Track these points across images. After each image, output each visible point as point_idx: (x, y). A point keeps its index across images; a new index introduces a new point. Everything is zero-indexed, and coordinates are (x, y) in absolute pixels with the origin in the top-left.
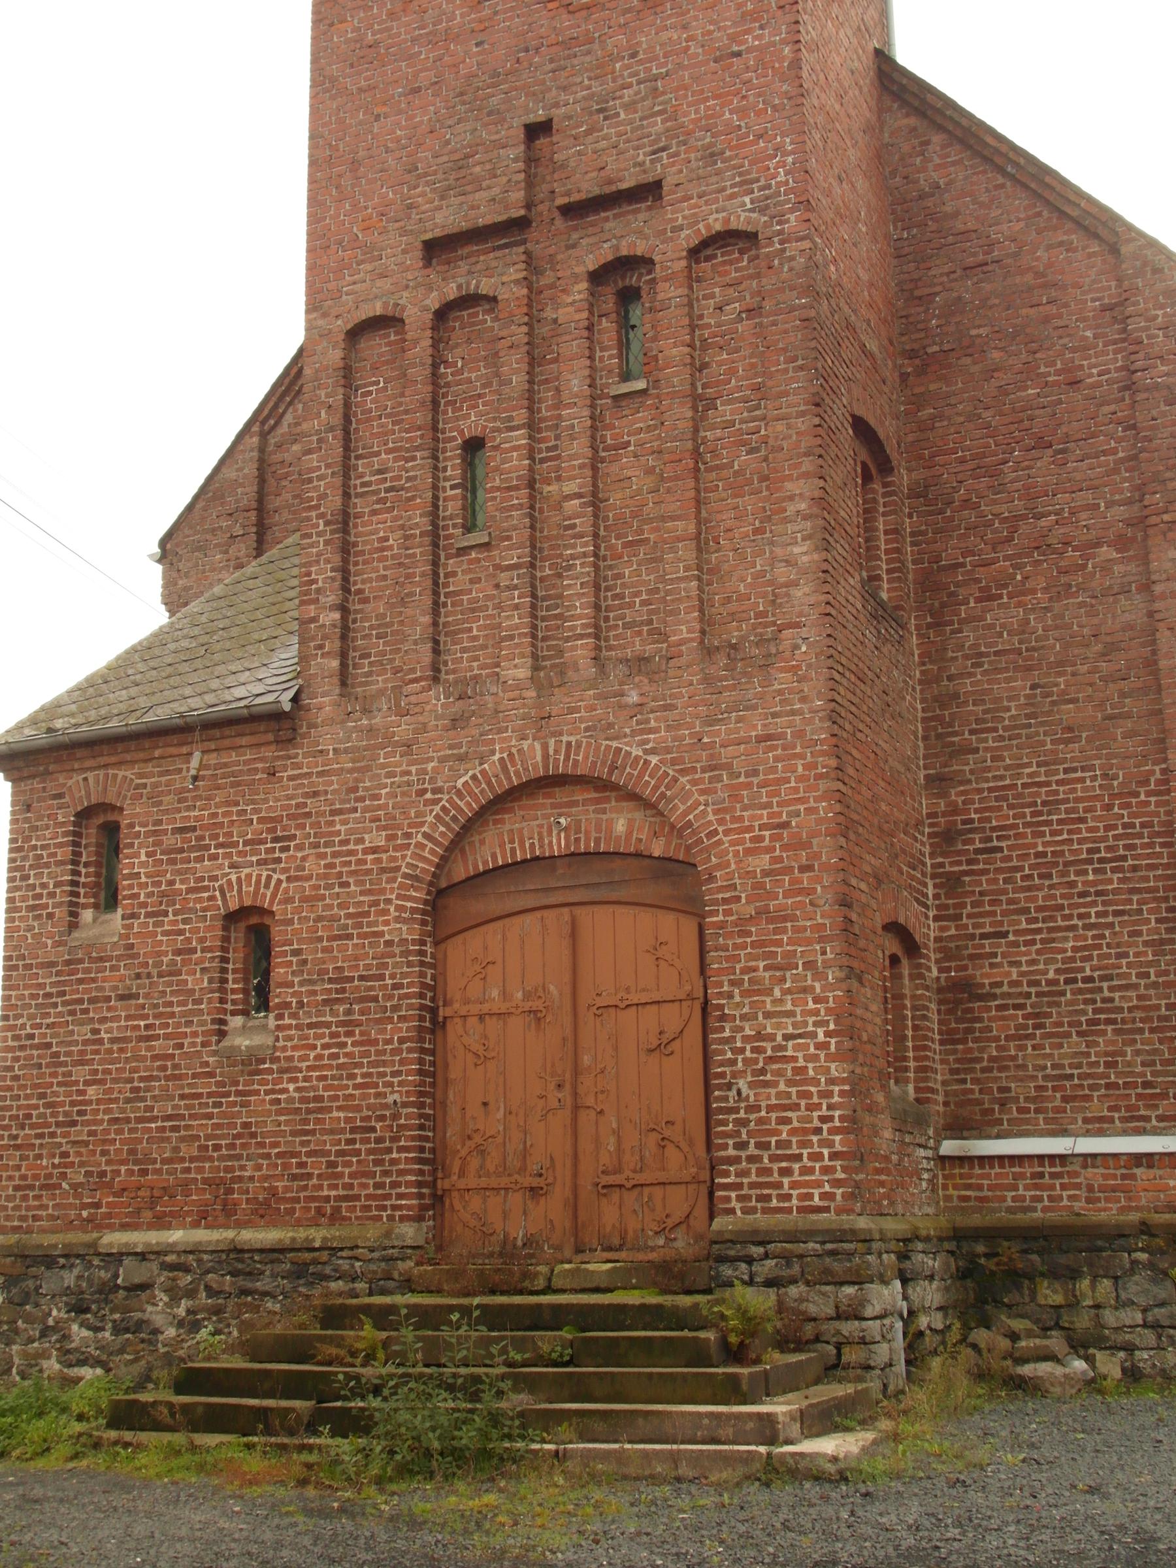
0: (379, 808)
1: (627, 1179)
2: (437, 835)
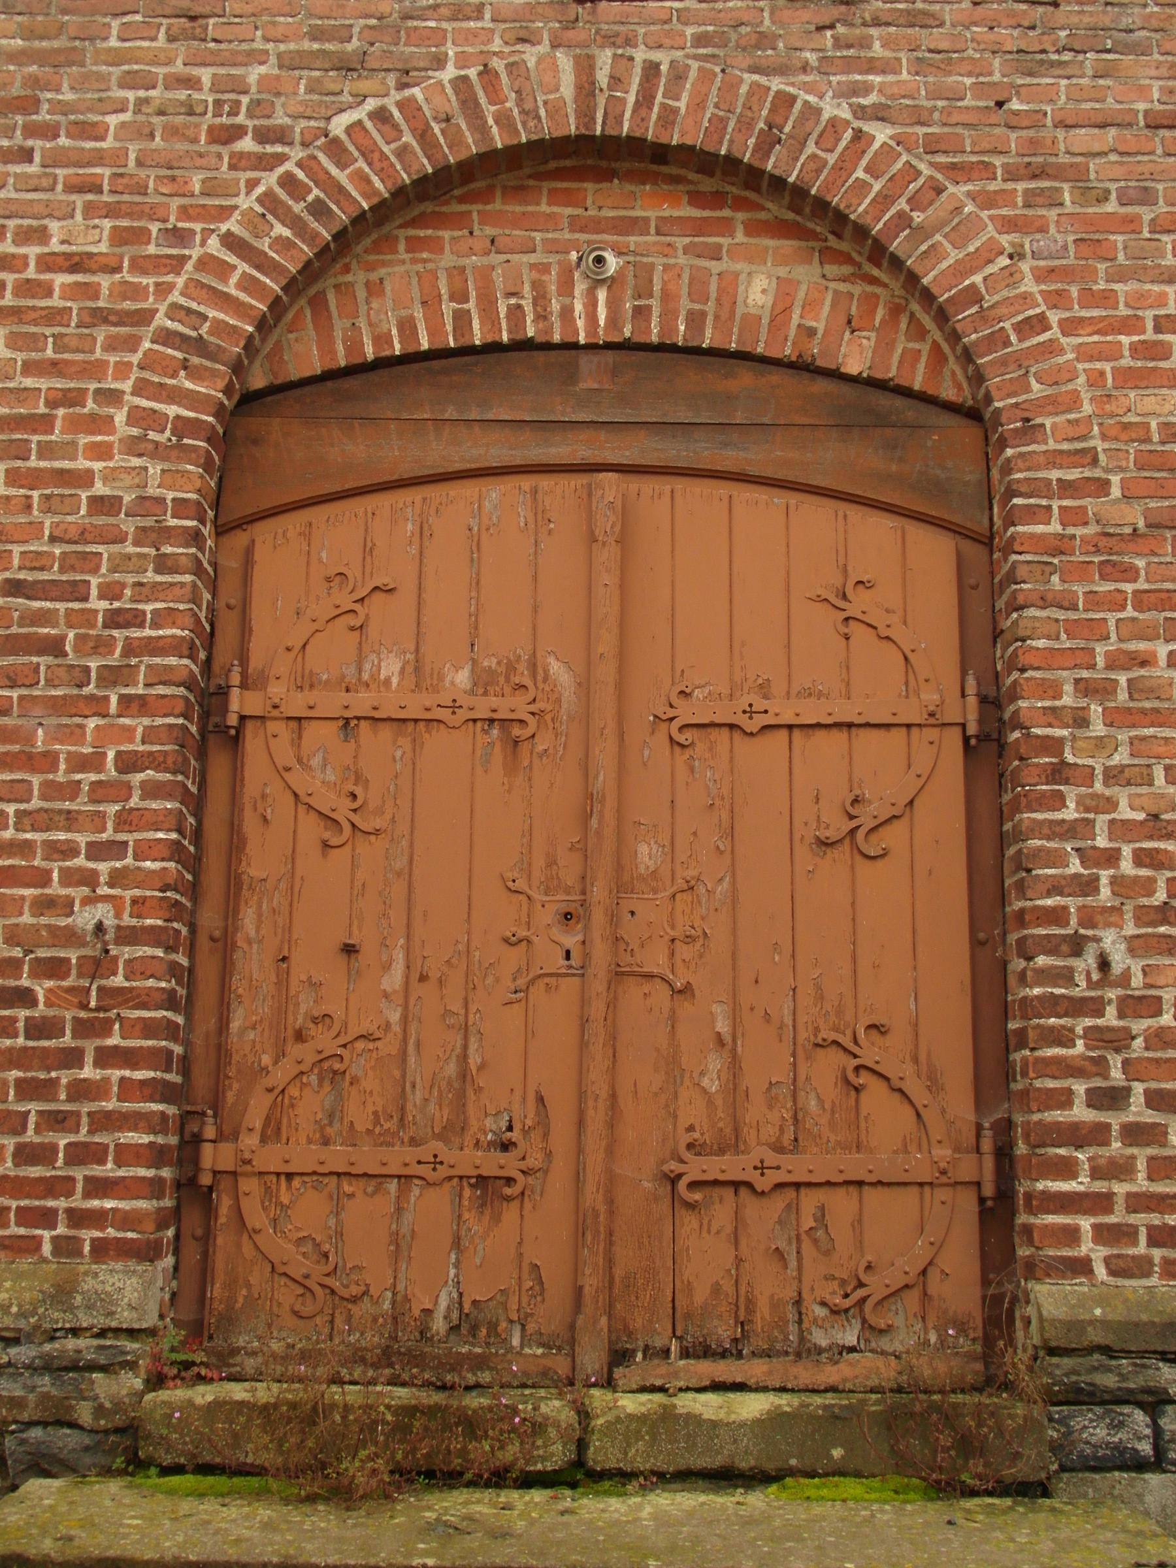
0: (99, 158)
1: (761, 1168)
2: (264, 245)
